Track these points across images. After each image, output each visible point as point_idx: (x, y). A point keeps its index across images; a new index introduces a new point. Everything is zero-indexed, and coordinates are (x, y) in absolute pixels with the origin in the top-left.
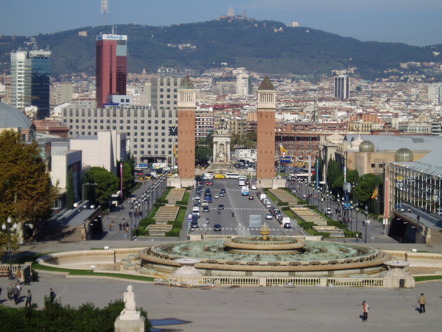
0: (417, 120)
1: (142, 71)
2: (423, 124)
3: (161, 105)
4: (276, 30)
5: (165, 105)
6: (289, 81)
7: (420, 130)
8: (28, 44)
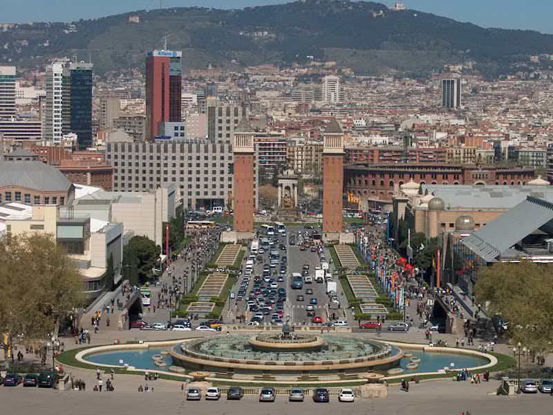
0: (531, 143)
1: (208, 66)
2: (538, 149)
3: (220, 139)
4: (375, 15)
5: (224, 139)
6: (391, 79)
7: (533, 156)
8: (67, 32)
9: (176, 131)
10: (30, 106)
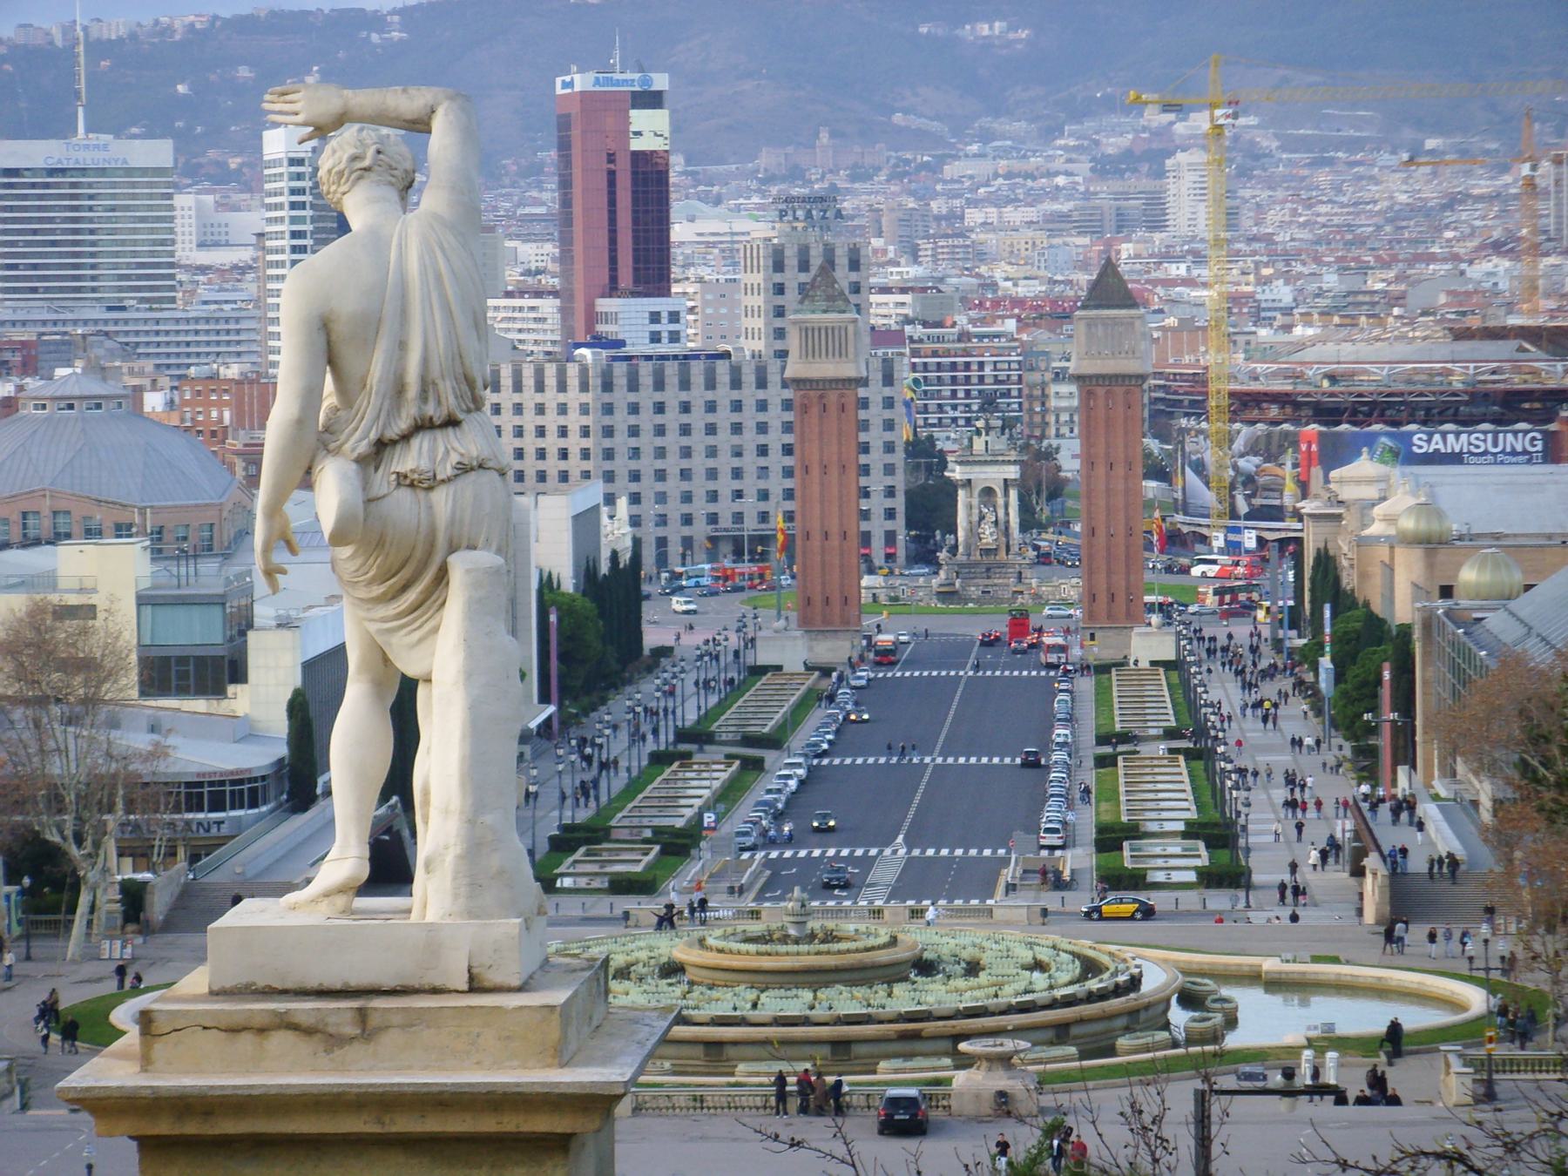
1: (817, 135)
8: (375, 37)
9: (656, 327)
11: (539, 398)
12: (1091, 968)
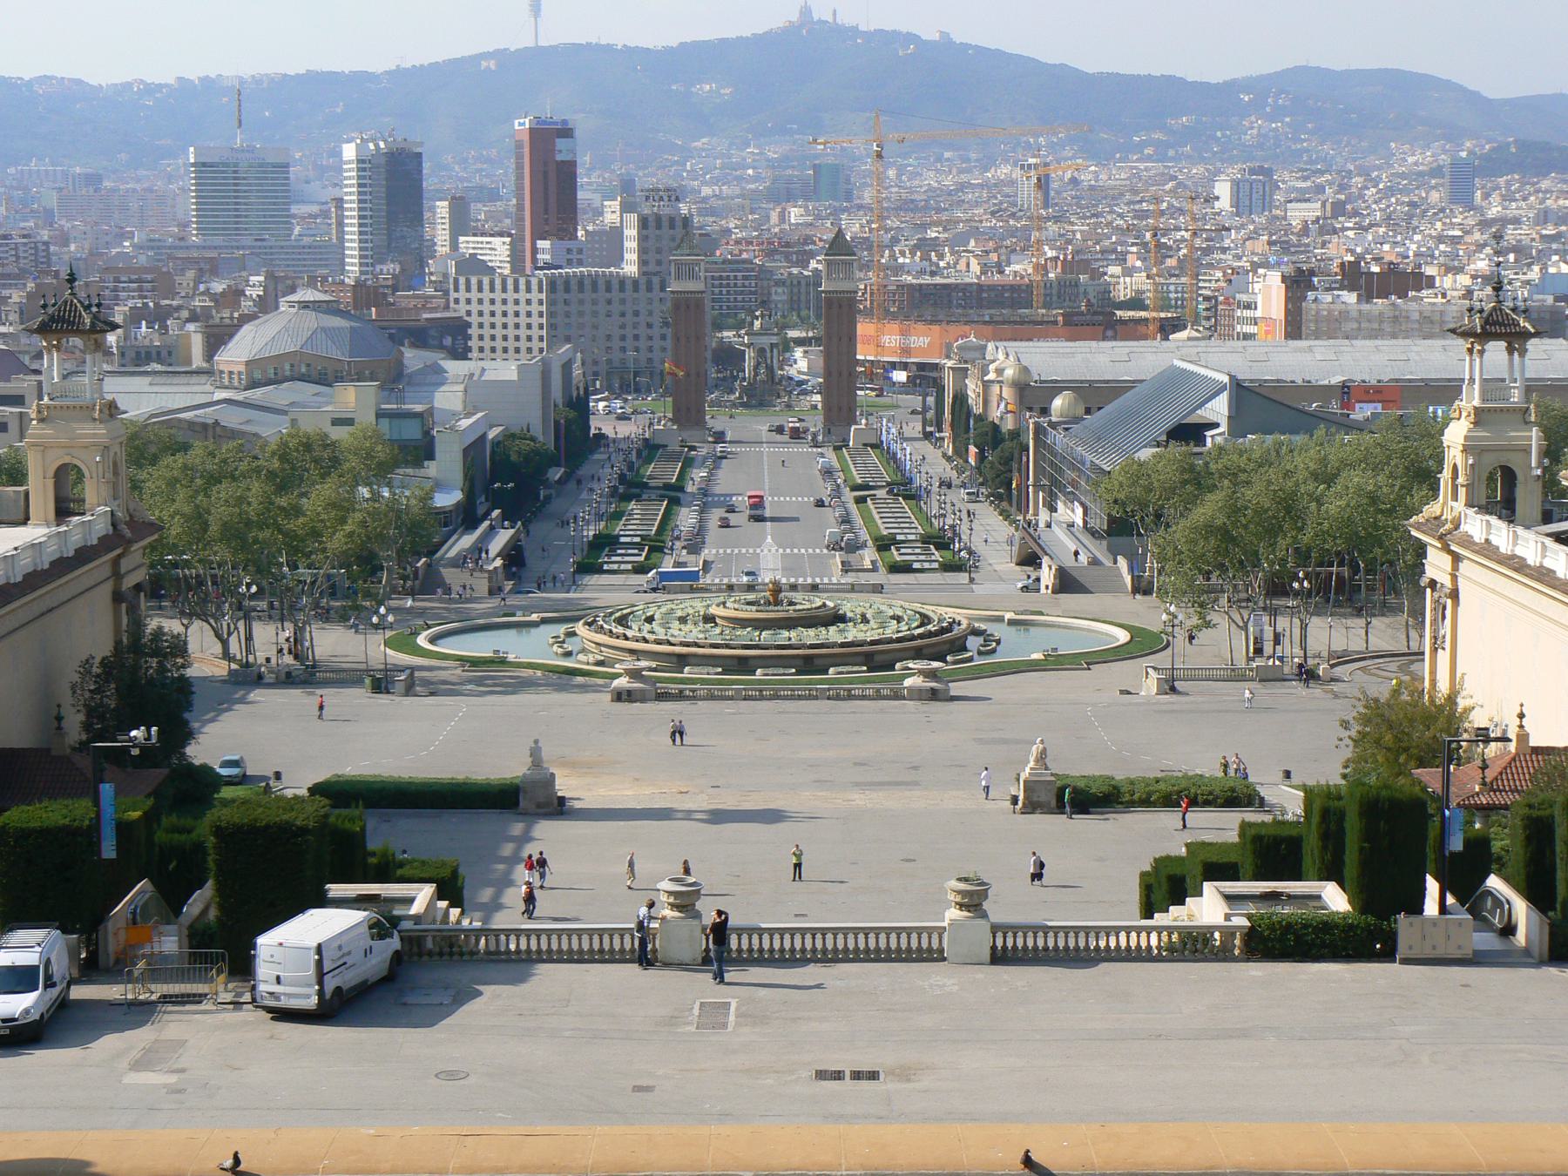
10: (316, 217)
11: (516, 296)
12: (925, 620)
